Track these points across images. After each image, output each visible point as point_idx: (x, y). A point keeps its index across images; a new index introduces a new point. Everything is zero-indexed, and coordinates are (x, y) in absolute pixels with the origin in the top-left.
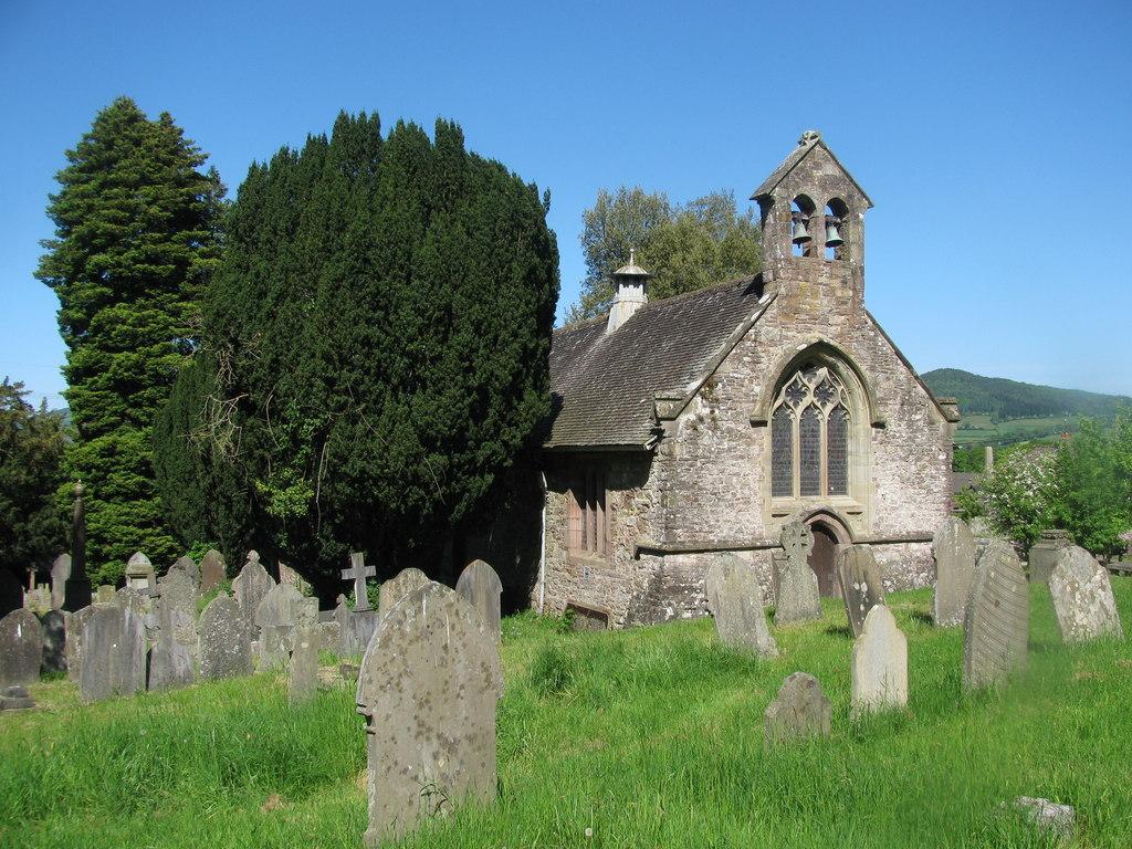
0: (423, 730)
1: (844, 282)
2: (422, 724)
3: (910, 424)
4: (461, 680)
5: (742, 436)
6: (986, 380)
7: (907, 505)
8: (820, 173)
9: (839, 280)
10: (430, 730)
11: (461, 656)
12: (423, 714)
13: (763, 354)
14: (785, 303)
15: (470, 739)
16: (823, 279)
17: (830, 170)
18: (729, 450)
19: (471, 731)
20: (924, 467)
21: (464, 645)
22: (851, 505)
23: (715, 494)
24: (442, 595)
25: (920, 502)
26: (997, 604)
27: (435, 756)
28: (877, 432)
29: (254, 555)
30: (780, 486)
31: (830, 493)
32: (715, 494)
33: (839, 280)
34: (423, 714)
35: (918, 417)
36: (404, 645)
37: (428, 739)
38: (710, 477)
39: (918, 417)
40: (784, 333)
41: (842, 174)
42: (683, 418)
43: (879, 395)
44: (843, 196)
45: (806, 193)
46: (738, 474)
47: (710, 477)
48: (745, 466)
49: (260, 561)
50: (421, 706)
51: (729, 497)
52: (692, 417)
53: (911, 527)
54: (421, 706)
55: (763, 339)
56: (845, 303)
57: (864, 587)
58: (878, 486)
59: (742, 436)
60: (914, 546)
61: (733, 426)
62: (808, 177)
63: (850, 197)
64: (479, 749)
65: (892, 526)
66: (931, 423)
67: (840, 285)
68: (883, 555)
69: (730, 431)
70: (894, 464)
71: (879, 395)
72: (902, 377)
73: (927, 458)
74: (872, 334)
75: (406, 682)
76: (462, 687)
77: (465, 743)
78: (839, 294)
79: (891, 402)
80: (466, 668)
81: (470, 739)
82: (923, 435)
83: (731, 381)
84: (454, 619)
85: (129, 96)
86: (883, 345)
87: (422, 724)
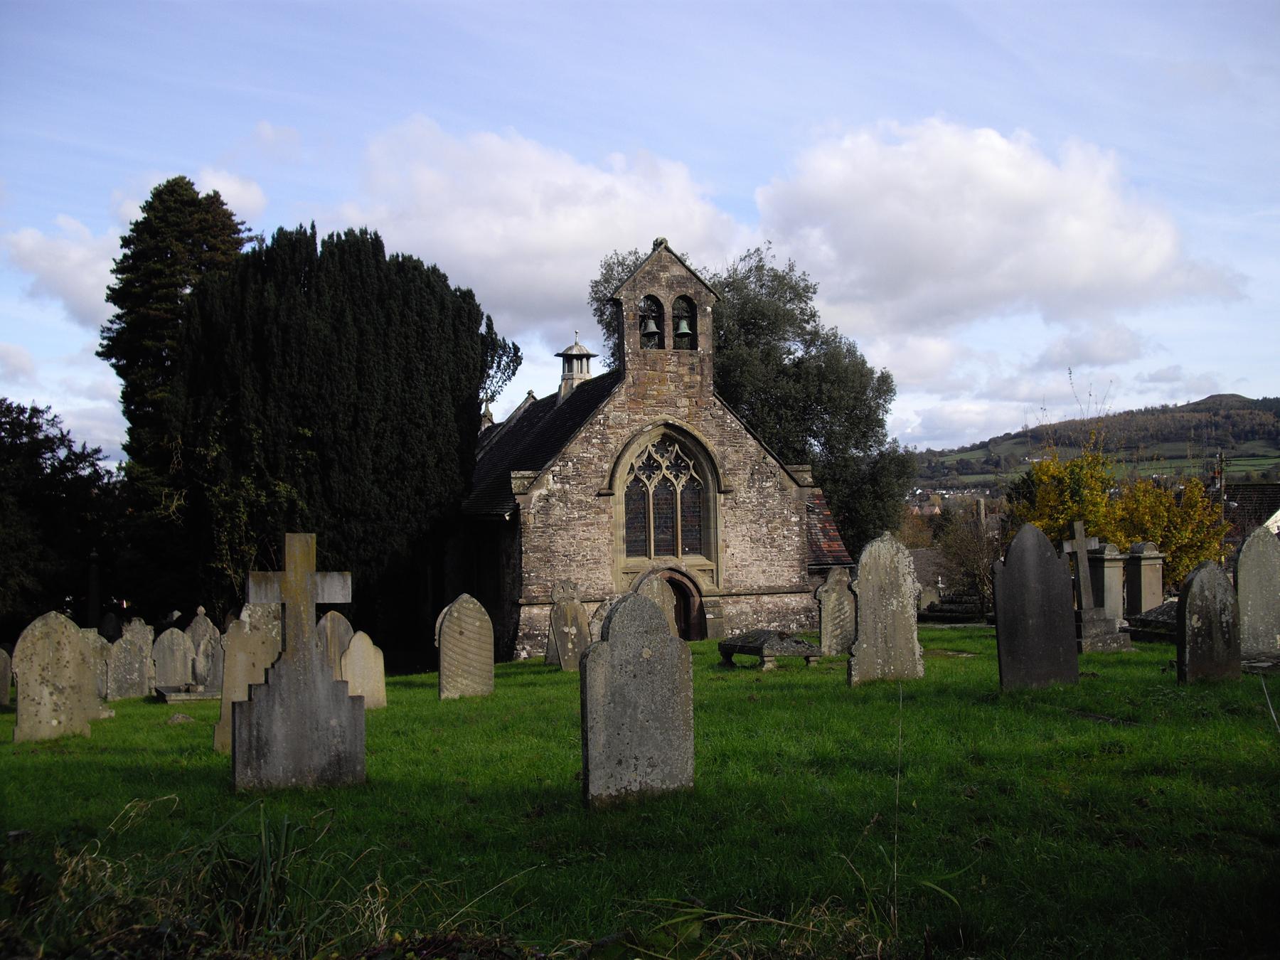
0: (44, 681)
1: (692, 369)
2: (43, 678)
3: (761, 490)
4: (67, 659)
5: (591, 507)
6: (1253, 400)
7: (758, 562)
8: (667, 275)
9: (686, 368)
10: (48, 681)
11: (68, 647)
12: (44, 674)
13: (612, 436)
14: (632, 390)
15: (72, 687)
16: (671, 368)
17: (677, 271)
18: (580, 518)
19: (73, 684)
20: (776, 529)
21: (70, 642)
22: (703, 563)
23: (566, 556)
24: (57, 618)
25: (772, 560)
26: (461, 633)
27: (51, 694)
28: (725, 499)
29: (201, 609)
30: (635, 546)
31: (684, 553)
32: (566, 556)
33: (686, 368)
34: (44, 674)
35: (768, 484)
36: (35, 640)
37: (47, 686)
38: (561, 542)
39: (768, 484)
40: (632, 417)
41: (689, 273)
42: (536, 493)
43: (728, 466)
44: (690, 292)
45: (653, 293)
46: (588, 539)
47: (561, 542)
48: (594, 532)
49: (206, 615)
50: (43, 670)
51: (579, 558)
52: (544, 492)
53: (762, 582)
54: (43, 670)
55: (611, 423)
56: (693, 387)
57: (574, 630)
58: (728, 547)
59: (591, 507)
60: (766, 599)
61: (583, 498)
62: (655, 279)
63: (698, 293)
64: (77, 693)
65: (742, 581)
66: (783, 489)
67: (688, 371)
68: (730, 609)
69: (580, 502)
70: (744, 527)
71: (728, 466)
72: (751, 449)
73: (779, 520)
74: (721, 413)
75: (34, 658)
76: (68, 662)
77: (69, 690)
78: (687, 379)
79: (740, 472)
80: (70, 652)
81: (72, 687)
82: (774, 501)
83: (580, 460)
84: (64, 629)
85: (190, 177)
86: (732, 422)
87: (43, 678)
